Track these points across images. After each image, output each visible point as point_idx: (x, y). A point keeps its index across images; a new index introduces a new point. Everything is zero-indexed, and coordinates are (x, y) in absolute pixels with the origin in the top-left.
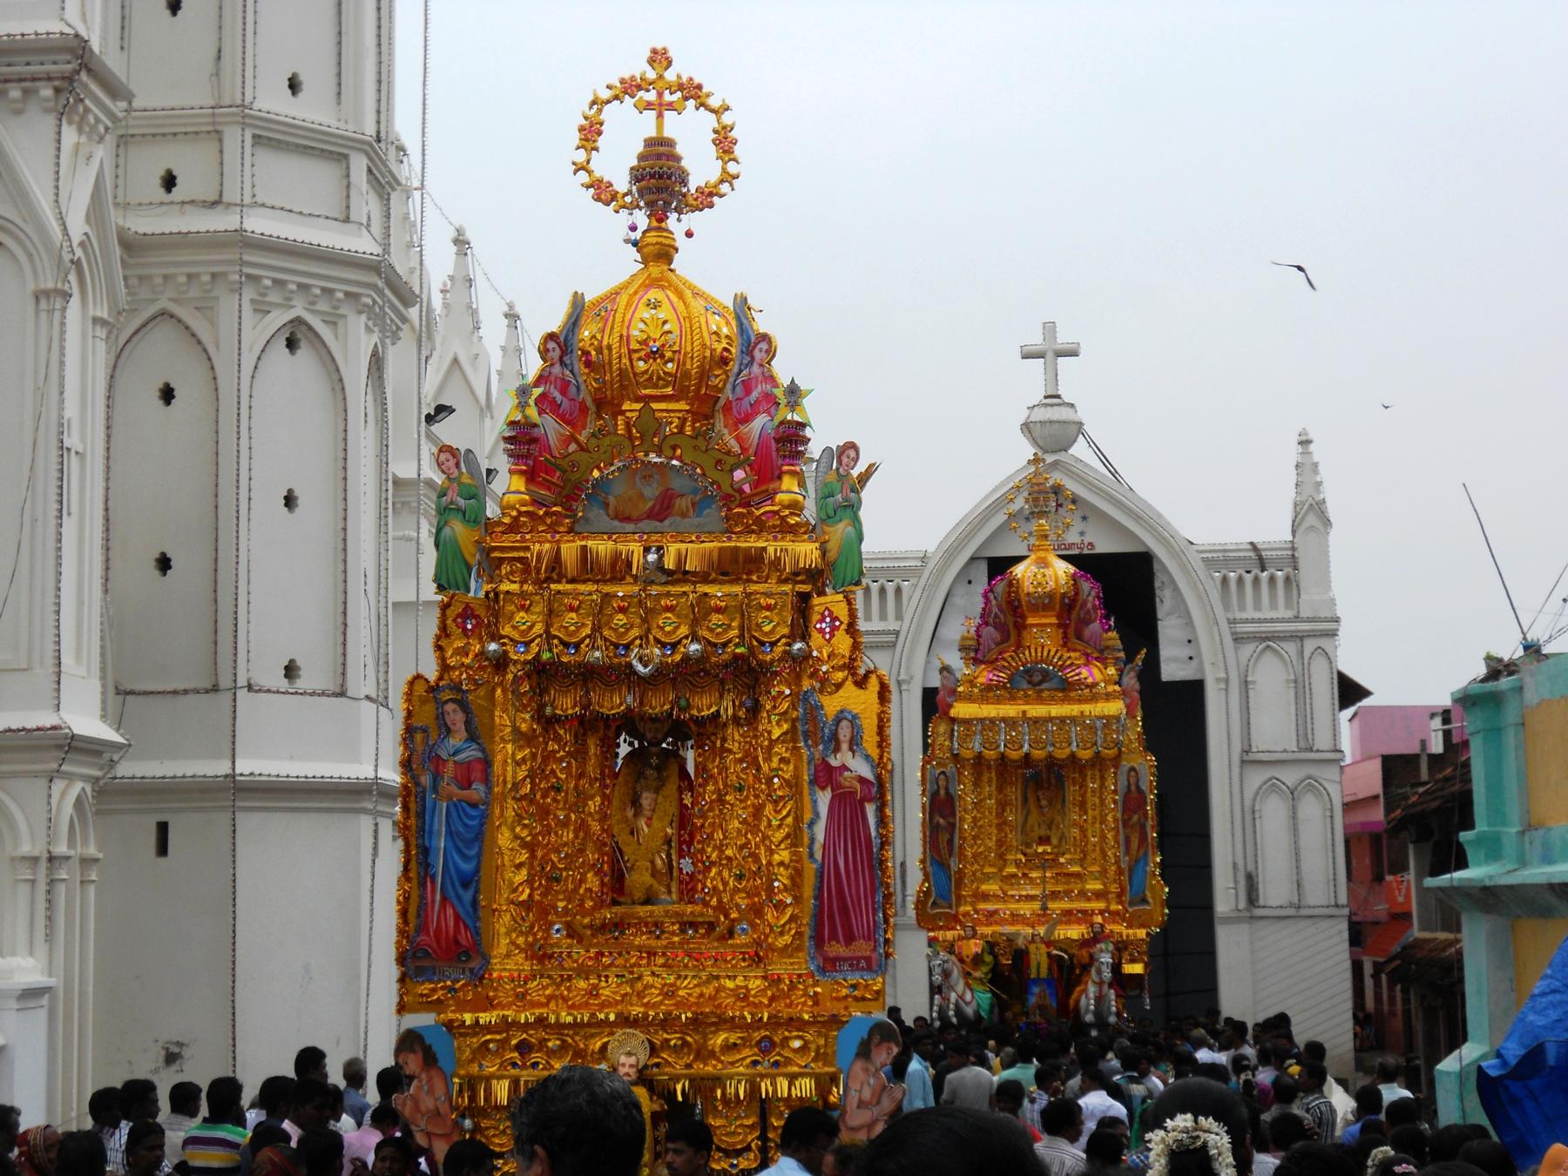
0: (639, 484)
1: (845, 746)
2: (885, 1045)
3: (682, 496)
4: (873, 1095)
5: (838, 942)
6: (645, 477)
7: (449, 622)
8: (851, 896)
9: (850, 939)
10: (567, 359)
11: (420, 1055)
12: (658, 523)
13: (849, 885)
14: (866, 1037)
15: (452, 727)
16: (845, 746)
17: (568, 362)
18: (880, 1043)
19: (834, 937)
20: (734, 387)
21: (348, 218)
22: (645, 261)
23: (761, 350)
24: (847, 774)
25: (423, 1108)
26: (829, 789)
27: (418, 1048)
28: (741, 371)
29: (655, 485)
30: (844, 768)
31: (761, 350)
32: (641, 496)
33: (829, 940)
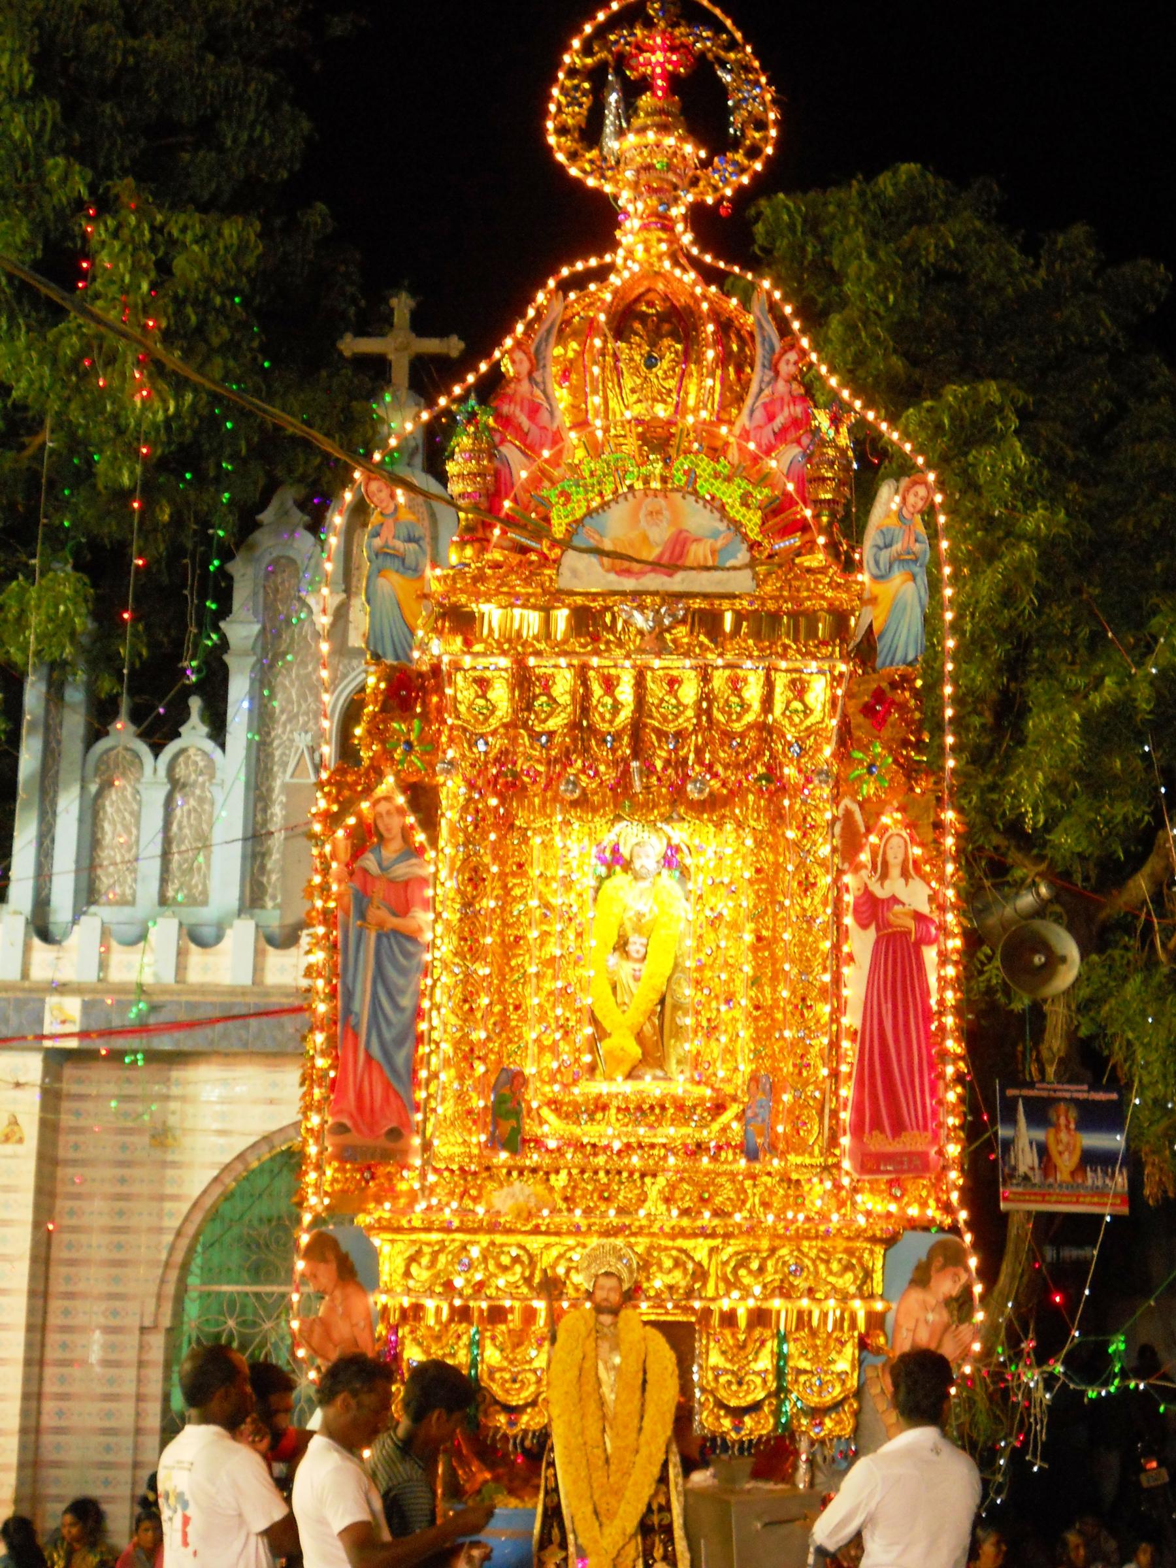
0: (643, 523)
1: (895, 872)
2: (951, 1270)
3: (698, 540)
4: (931, 1336)
5: (883, 1131)
6: (651, 513)
7: (102, 329)
8: (901, 1071)
9: (898, 1128)
10: (537, 376)
11: (333, 1266)
12: (666, 579)
13: (899, 1061)
14: (924, 1258)
15: (386, 835)
16: (895, 872)
17: (539, 379)
18: (944, 1267)
19: (876, 1124)
20: (752, 412)
21: (500, 1116)
22: (310, 1006)
23: (788, 362)
24: (897, 908)
25: (336, 1336)
26: (873, 928)
27: (331, 1256)
28: (761, 390)
29: (665, 524)
30: (894, 900)
31: (788, 362)
32: (645, 539)
33: (871, 1129)
